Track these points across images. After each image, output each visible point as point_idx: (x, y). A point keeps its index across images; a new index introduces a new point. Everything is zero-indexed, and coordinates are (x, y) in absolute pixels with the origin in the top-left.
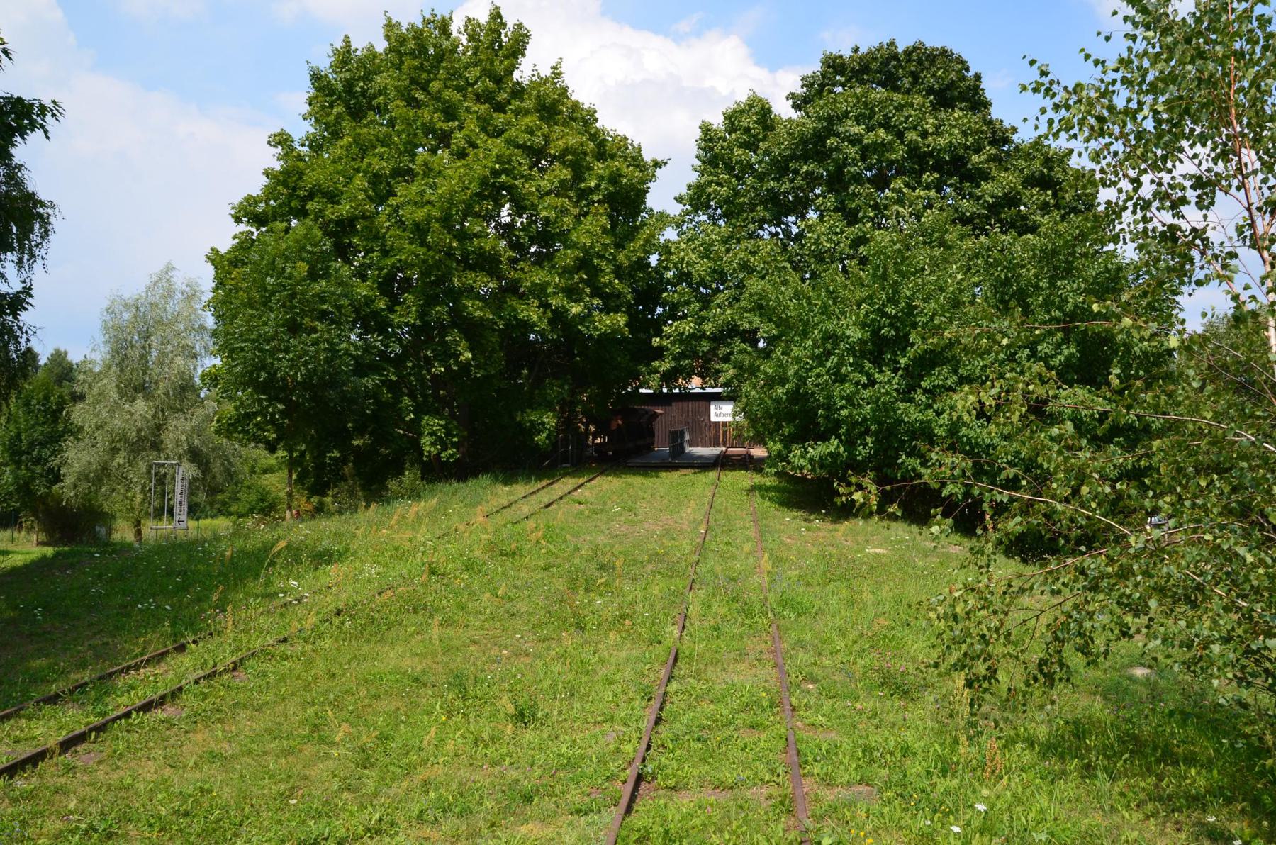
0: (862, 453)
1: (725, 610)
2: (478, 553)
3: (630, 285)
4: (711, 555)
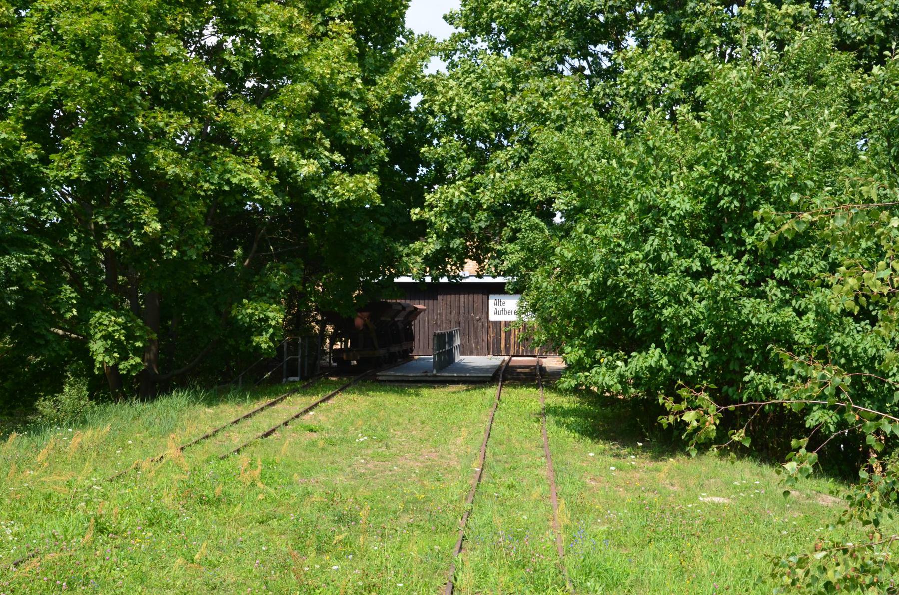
0: (692, 365)
1: (507, 578)
2: (167, 500)
3: (382, 136)
4: (489, 503)
